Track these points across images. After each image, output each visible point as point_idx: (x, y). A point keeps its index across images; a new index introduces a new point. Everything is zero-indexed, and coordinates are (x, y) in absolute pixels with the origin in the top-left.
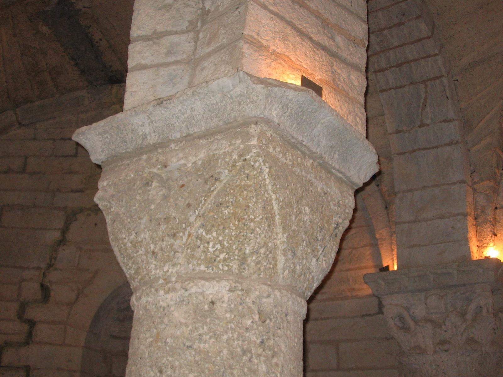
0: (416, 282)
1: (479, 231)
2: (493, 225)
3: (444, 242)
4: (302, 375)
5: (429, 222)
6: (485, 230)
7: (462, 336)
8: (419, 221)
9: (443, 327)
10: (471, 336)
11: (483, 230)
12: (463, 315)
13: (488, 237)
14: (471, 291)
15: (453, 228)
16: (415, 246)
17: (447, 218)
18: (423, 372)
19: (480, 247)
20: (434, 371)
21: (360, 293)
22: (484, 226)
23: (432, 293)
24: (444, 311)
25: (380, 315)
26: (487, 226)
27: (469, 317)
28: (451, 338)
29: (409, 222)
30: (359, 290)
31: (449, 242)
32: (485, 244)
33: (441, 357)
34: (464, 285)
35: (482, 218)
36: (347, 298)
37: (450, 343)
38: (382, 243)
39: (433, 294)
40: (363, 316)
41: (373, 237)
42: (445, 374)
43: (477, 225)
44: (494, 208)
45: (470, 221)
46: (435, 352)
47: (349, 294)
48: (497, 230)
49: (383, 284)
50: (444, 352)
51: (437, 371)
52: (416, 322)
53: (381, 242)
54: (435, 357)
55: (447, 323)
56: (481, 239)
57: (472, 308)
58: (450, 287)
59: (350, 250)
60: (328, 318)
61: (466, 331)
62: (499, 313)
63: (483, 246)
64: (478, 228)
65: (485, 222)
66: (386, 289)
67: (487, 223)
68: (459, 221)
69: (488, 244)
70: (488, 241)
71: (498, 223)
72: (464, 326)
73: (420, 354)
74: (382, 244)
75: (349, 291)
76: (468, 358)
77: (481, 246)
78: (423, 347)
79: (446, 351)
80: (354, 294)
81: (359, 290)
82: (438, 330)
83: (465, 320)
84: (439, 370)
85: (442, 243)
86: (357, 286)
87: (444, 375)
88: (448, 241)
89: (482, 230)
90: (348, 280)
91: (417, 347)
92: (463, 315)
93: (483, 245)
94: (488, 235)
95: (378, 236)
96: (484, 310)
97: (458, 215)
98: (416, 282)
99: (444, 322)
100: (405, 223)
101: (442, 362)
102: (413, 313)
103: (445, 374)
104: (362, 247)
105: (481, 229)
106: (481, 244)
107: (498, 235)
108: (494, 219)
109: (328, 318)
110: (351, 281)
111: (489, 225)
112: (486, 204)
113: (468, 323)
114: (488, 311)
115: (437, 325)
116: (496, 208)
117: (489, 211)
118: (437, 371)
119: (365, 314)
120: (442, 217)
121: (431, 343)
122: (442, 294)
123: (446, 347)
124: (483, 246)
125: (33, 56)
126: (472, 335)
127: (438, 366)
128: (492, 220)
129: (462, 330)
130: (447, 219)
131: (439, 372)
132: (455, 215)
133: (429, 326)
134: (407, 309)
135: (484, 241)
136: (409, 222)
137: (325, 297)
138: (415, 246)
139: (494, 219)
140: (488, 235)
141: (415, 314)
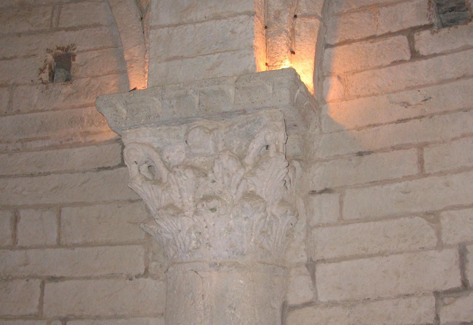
0: (172, 107)
1: (270, 44)
2: (291, 39)
3: (218, 53)
4: (279, 322)
5: (198, 25)
6: (278, 43)
7: (237, 188)
8: (184, 24)
9: (210, 175)
10: (250, 189)
11: (276, 43)
12: (240, 158)
13: (283, 52)
14: (254, 121)
15: (233, 32)
16: (176, 58)
17: (225, 18)
18: (178, 244)
19: (270, 66)
20: (194, 242)
21: (98, 138)
22: (278, 37)
23: (196, 126)
24: (213, 152)
25: (123, 168)
26: (282, 37)
27: (249, 160)
28: (221, 192)
29: (169, 26)
30: (96, 133)
31: (226, 51)
32: (277, 61)
33: (205, 220)
34: (244, 112)
35: (276, 27)
36: (78, 145)
37: (218, 198)
38: (132, 66)
39: (197, 127)
40: (100, 169)
41: (122, 61)
42: (210, 246)
43: (267, 36)
44: (293, 16)
45: (258, 25)
46: (196, 213)
47: (81, 139)
48: (295, 46)
49: (124, 111)
50: (210, 212)
51: (198, 241)
52: (169, 168)
53: (131, 64)
54: (196, 220)
55: (216, 169)
56: (272, 55)
57: (255, 146)
58: (224, 115)
59: (88, 79)
60: (49, 173)
61: (244, 181)
62: (294, 160)
63: (275, 65)
64: (269, 40)
65: (279, 32)
66: (129, 119)
67: (281, 33)
68: (242, 23)
69: (282, 61)
70: (282, 58)
71: (297, 36)
72: (242, 172)
73: (174, 215)
74: (133, 67)
75: (82, 136)
76: (245, 223)
77: (271, 65)
78: (180, 206)
79: (213, 210)
80: (89, 139)
81: (96, 133)
82: (202, 180)
83: (243, 165)
84: (201, 240)
85: (214, 54)
86: (93, 129)
87: (208, 247)
88: (224, 50)
89: (274, 42)
90: (82, 120)
91: (171, 206)
92: (240, 158)
93: (275, 63)
94: (283, 50)
95: (126, 57)
96: (272, 148)
97: (240, 14)
98: (172, 107)
99: (212, 168)
100: (163, 27)
101: (206, 227)
102: (168, 157)
103: (210, 246)
104: (104, 75)
105: (273, 41)
106: (272, 62)
107: (297, 53)
108: (293, 30)
109: (49, 173)
110: (86, 121)
111: (285, 36)
112: (282, 8)
113: (247, 170)
114: (277, 151)
115: (201, 172)
116: (295, 16)
117: (286, 17)
118: (198, 241)
119: (101, 166)
120: (217, 17)
121: (191, 199)
122: (210, 128)
123: (213, 204)
124: (275, 65)
125: (193, 253)
126: (252, 188)
127: (200, 233)
128: (289, 30)
129: (238, 180)
130: (225, 21)
131: (200, 243)
132: (236, 15)
133: (190, 174)
134: (160, 151)
135: (276, 58)
136: (169, 26)
137: (47, 144)
138: (176, 58)
139: (293, 30)
140: (283, 50)
141: (170, 159)
